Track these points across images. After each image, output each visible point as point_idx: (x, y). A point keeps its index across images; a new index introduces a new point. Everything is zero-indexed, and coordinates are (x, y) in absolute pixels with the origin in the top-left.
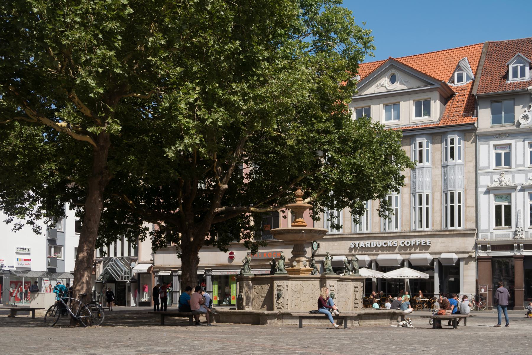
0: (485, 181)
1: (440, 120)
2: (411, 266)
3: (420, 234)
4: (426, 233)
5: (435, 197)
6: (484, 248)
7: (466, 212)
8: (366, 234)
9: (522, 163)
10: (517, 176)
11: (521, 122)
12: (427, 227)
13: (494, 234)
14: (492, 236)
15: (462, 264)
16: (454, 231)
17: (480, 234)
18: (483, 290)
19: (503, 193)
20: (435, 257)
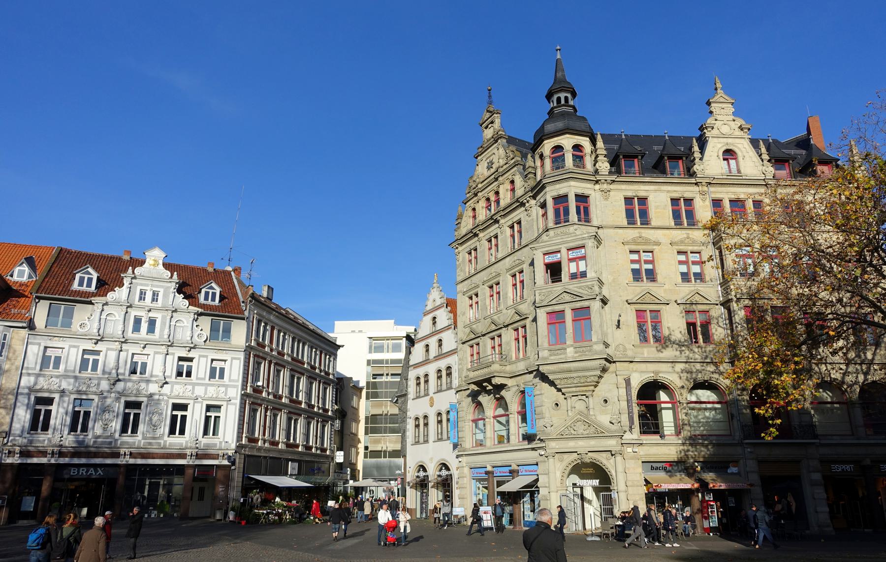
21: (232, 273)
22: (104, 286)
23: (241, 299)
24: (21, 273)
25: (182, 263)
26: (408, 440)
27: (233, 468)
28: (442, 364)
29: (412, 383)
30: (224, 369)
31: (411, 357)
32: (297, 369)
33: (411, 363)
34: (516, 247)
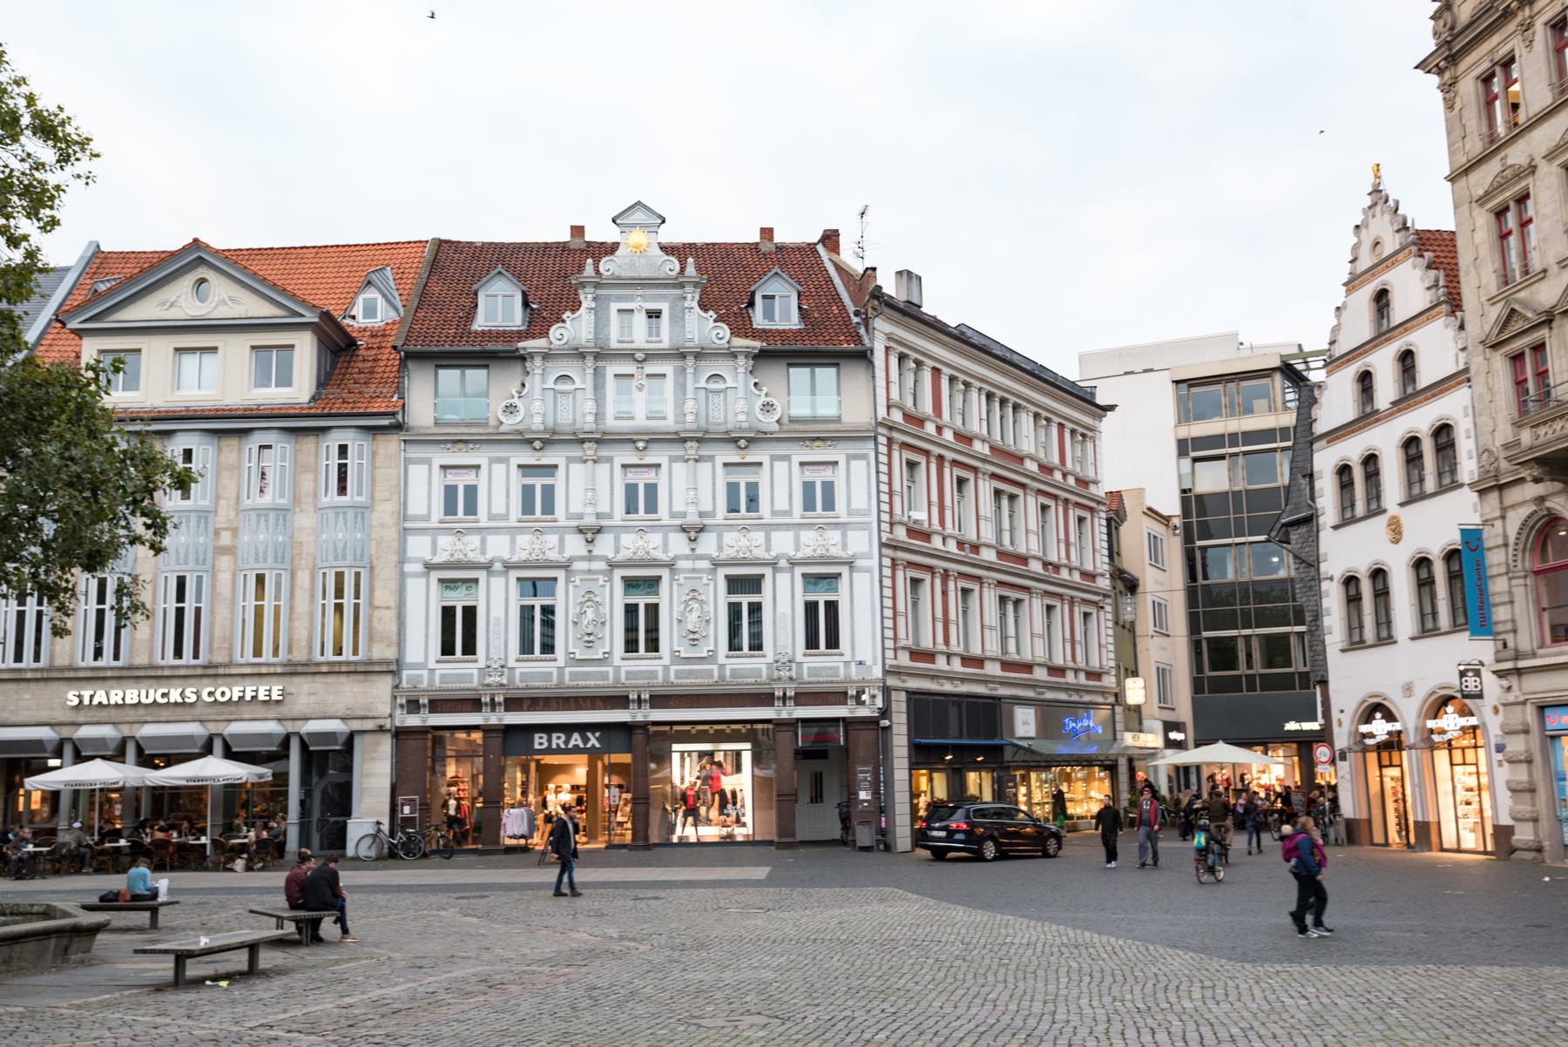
0: (419, 547)
1: (313, 399)
2: (229, 754)
3: (256, 670)
4: (272, 670)
5: (299, 582)
6: (413, 706)
7: (370, 621)
8: (112, 669)
9: (503, 511)
10: (776, 536)
11: (503, 419)
12: (196, 656)
13: (438, 673)
14: (431, 680)
15: (357, 741)
16: (340, 663)
17: (405, 673)
18: (407, 810)
19: (456, 574)
20: (213, 731)
21: (820, 248)
22: (540, 318)
23: (851, 309)
24: (370, 311)
25: (700, 239)
26: (1328, 639)
27: (885, 723)
28: (1421, 420)
29: (1326, 486)
30: (832, 483)
31: (1316, 412)
32: (1009, 475)
33: (1319, 428)
34: (1501, 129)
